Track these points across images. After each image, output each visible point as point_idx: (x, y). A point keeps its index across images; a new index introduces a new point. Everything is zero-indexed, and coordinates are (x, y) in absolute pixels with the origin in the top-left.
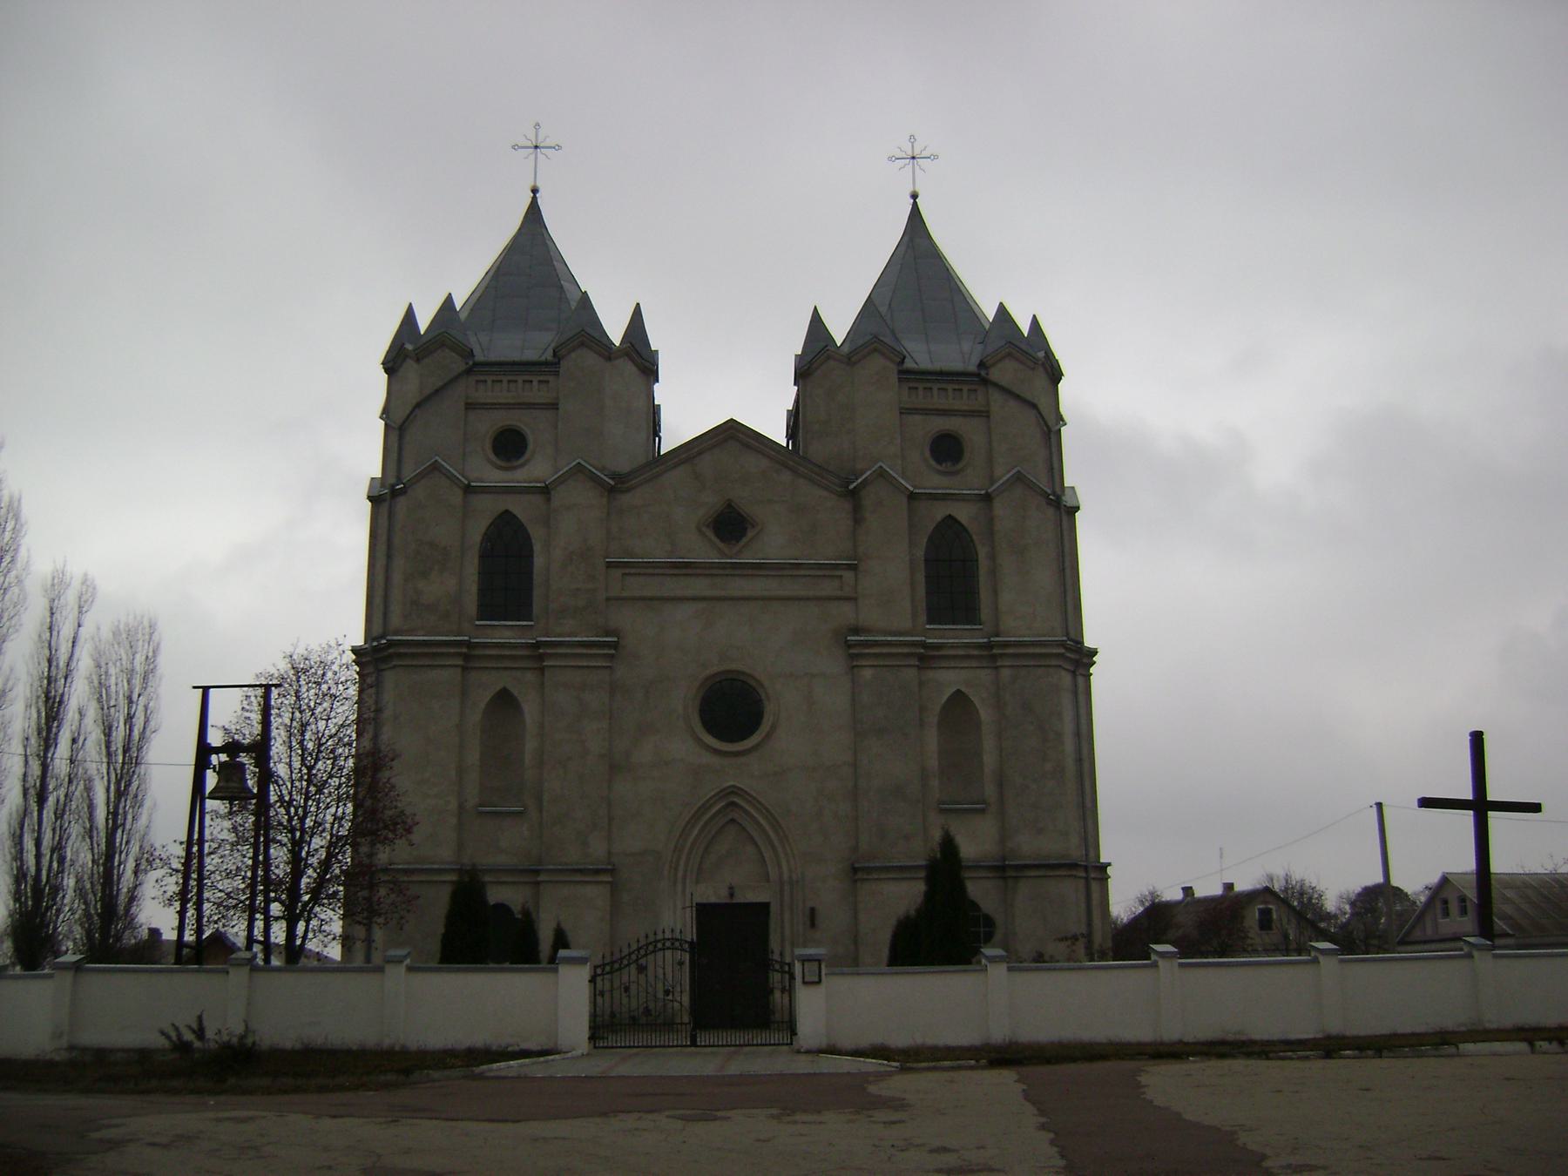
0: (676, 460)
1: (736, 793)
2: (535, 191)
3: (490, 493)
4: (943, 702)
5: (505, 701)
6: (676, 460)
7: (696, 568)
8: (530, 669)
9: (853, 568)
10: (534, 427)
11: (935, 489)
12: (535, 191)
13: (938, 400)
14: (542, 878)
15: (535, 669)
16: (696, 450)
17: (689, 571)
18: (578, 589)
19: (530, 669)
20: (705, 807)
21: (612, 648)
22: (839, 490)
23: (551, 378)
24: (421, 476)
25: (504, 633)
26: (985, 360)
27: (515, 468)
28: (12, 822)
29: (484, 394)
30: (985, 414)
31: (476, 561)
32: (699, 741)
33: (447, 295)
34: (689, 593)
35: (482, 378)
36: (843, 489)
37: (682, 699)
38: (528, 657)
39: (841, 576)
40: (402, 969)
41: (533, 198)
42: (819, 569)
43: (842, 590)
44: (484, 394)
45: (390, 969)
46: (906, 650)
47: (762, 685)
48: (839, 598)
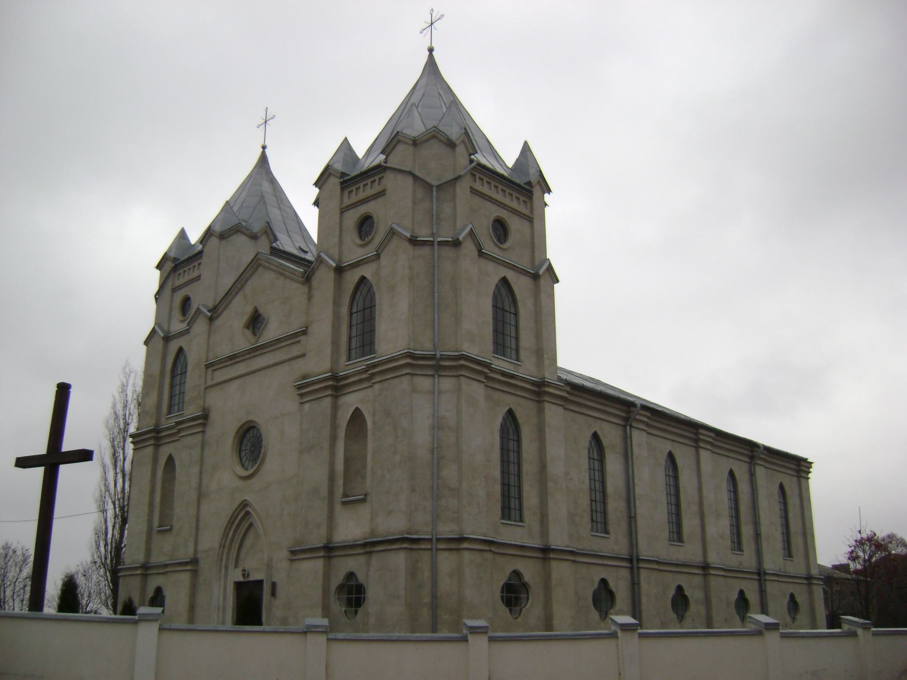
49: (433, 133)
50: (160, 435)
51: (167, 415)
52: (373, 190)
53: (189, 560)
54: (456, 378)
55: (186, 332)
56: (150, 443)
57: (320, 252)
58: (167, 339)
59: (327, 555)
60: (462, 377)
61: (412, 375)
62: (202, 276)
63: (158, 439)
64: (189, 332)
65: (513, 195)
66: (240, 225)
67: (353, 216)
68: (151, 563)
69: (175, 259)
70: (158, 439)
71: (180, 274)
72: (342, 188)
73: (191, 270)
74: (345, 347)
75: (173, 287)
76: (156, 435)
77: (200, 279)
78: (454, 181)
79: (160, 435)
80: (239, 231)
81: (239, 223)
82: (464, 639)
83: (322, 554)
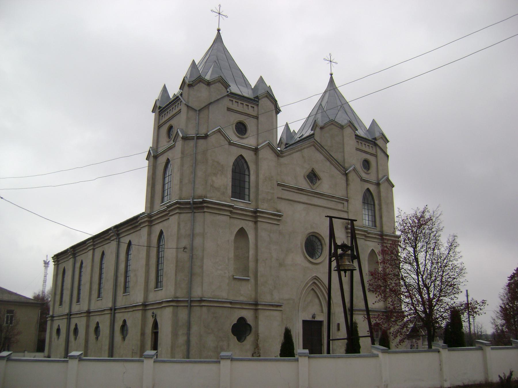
0: (298, 149)
1: (317, 280)
2: (331, 75)
3: (235, 146)
4: (369, 252)
5: (242, 233)
6: (298, 149)
7: (304, 191)
8: (251, 221)
9: (347, 201)
10: (251, 124)
11: (365, 178)
12: (331, 75)
13: (240, 108)
14: (259, 307)
15: (252, 221)
16: (303, 147)
17: (302, 192)
18: (268, 192)
19: (251, 221)
20: (307, 283)
21: (277, 216)
22: (343, 172)
23: (255, 107)
24: (214, 133)
25: (240, 204)
26: (259, 96)
27: (243, 138)
28: (320, 247)
29: (235, 106)
30: (376, 156)
31: (231, 172)
32: (306, 257)
33: (259, 77)
34: (301, 200)
35: (232, 99)
36: (344, 172)
37: (300, 240)
38: (252, 216)
39: (343, 203)
40: (152, 361)
41: (331, 77)
42: (338, 199)
43: (344, 208)
44: (235, 106)
45: (146, 361)
46: (363, 233)
47: (323, 239)
48: (343, 211)
49: (199, 79)
50: (119, 232)
51: (161, 204)
52: (178, 108)
53: (86, 311)
54: (203, 213)
55: (170, 148)
56: (146, 225)
57: (178, 129)
58: (156, 157)
59: (144, 308)
60: (206, 213)
61: (180, 213)
62: (182, 110)
63: (150, 222)
64: (175, 146)
65: (244, 104)
66: (200, 77)
67: (165, 129)
68: (112, 306)
69: (160, 107)
70: (150, 222)
71: (163, 116)
72: (159, 114)
73: (171, 111)
74: (161, 196)
75: (159, 125)
76: (149, 219)
77: (181, 112)
78: (208, 106)
79: (119, 232)
80: (200, 81)
81: (200, 76)
82: (219, 362)
83: (141, 308)
